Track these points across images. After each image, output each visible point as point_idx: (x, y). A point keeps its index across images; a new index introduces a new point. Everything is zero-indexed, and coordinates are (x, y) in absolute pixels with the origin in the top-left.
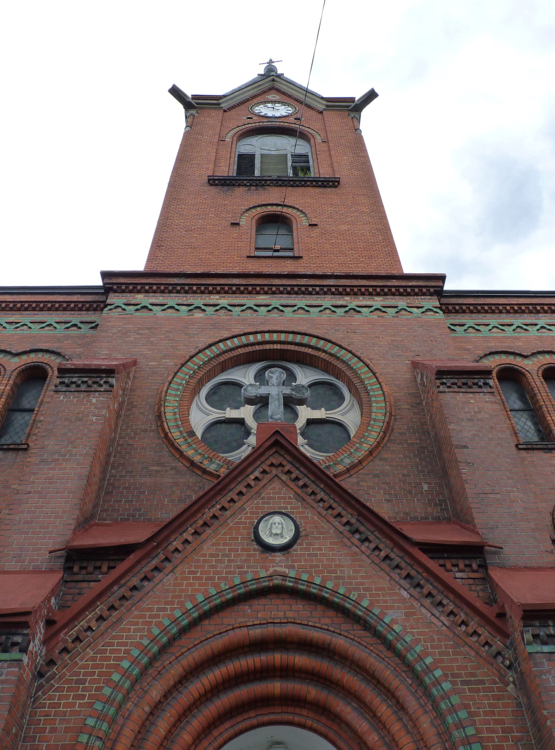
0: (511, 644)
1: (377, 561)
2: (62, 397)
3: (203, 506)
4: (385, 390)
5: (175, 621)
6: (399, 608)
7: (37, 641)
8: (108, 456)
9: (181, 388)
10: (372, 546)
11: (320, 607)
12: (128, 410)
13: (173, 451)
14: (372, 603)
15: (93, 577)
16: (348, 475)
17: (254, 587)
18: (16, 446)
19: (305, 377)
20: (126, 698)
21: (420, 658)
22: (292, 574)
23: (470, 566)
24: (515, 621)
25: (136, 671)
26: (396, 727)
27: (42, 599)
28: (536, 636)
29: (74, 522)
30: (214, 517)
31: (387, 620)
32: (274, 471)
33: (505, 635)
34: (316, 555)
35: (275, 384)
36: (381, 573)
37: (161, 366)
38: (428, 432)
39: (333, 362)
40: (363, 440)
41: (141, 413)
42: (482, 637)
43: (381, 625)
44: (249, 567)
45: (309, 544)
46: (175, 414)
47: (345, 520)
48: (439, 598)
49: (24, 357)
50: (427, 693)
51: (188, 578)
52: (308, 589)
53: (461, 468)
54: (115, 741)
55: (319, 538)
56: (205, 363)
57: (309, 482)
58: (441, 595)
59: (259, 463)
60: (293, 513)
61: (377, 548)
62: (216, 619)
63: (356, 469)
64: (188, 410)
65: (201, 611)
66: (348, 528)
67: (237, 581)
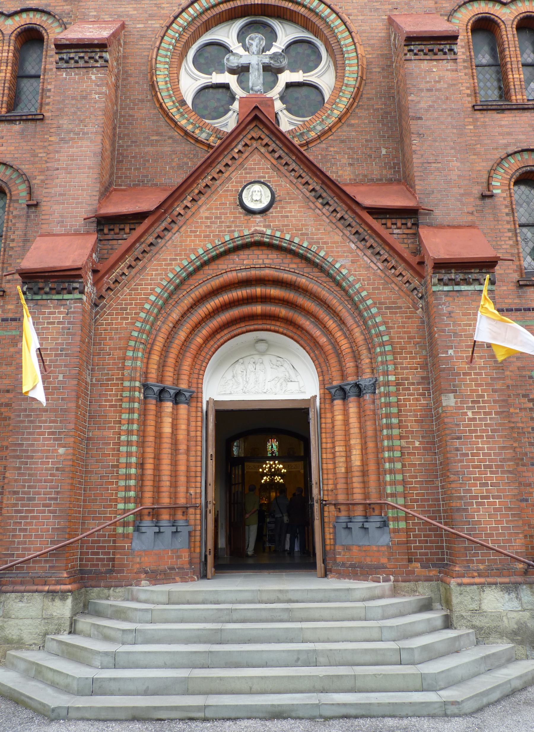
0: (425, 283)
1: (334, 220)
2: (64, 74)
3: (197, 178)
4: (359, 52)
5: (184, 268)
6: (347, 256)
7: (89, 285)
8: (114, 128)
9: (169, 53)
10: (331, 209)
11: (289, 256)
12: (124, 79)
13: (168, 121)
14: (327, 253)
15: (120, 236)
16: (319, 141)
17: (240, 242)
18: (33, 117)
19: (286, 34)
20: (156, 318)
21: (358, 292)
22: (269, 232)
23: (406, 224)
24: (429, 268)
25: (160, 302)
26: (338, 334)
27: (86, 257)
28: (440, 280)
29: (97, 194)
30: (207, 186)
31: (337, 266)
32: (255, 144)
33: (421, 276)
34: (287, 216)
35: (255, 53)
36: (337, 230)
37: (149, 29)
38: (393, 97)
39: (312, 19)
40: (334, 106)
41: (137, 83)
42: (405, 278)
43: (333, 270)
44: (236, 226)
45: (283, 207)
46: (166, 83)
47: (311, 187)
48: (378, 249)
49: (17, 18)
50: (361, 314)
51: (191, 236)
52: (280, 243)
53: (413, 139)
54: (153, 344)
55: (290, 203)
56: (189, 24)
57: (283, 155)
58: (379, 247)
59: (241, 137)
60: (270, 181)
61: (335, 210)
62: (213, 266)
63: (326, 136)
64: (178, 74)
65: (202, 261)
66: (313, 194)
67: (227, 238)
